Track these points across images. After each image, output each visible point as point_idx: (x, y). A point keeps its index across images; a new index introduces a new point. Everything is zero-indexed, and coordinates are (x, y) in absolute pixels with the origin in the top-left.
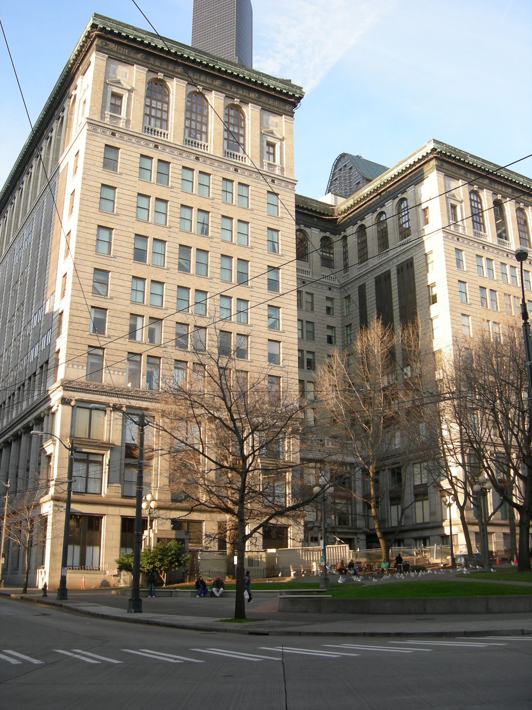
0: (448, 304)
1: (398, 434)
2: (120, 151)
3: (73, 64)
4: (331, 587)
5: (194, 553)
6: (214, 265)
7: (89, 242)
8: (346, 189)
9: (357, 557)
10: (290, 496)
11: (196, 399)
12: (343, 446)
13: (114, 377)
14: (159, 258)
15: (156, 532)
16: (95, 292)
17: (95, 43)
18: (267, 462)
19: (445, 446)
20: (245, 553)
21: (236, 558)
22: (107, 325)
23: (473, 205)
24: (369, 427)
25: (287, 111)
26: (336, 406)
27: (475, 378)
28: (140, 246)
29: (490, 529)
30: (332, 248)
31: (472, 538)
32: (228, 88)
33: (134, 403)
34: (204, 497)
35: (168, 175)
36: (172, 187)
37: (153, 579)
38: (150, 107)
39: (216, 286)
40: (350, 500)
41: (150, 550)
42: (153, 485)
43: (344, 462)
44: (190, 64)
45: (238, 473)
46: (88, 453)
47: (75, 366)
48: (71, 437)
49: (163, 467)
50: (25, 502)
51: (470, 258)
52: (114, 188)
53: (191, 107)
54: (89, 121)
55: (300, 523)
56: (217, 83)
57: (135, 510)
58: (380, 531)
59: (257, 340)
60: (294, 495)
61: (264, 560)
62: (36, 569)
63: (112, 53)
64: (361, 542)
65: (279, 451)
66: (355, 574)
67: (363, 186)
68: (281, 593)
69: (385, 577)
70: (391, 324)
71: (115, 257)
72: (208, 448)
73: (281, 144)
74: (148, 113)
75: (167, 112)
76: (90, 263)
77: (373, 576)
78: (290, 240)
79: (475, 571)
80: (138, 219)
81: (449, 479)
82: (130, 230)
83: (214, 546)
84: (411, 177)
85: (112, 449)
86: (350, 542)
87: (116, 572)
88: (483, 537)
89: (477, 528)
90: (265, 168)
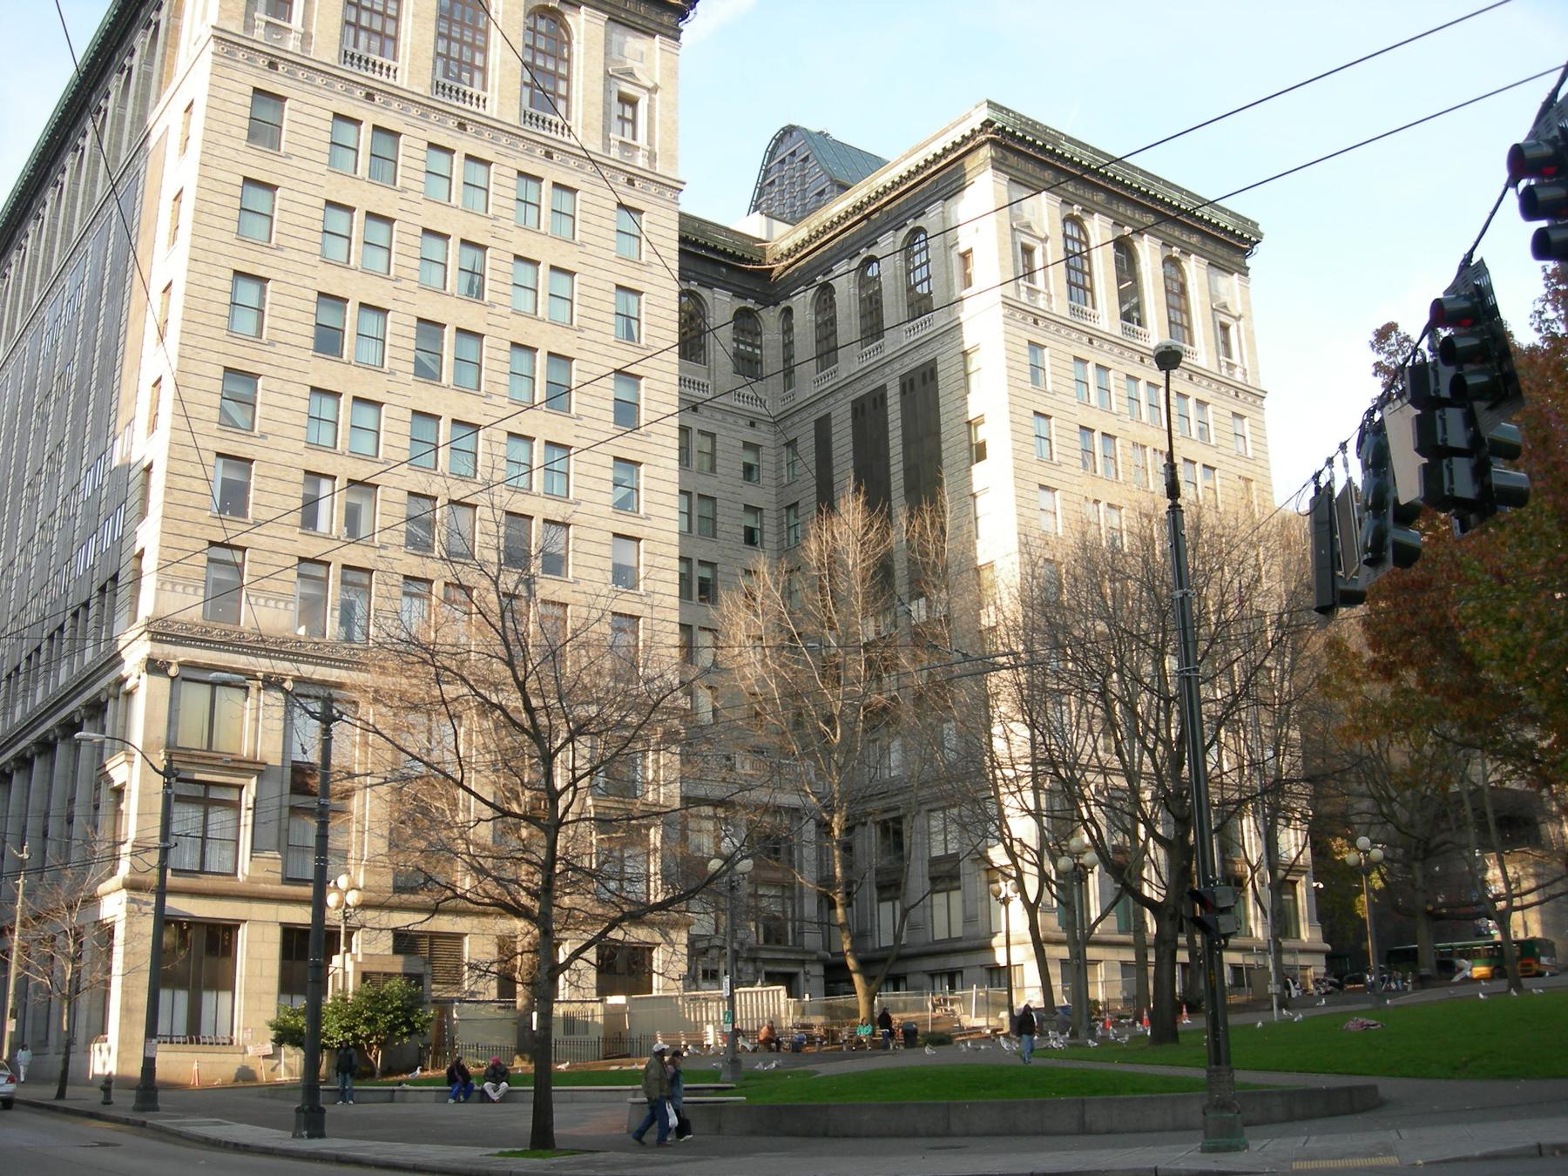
1: (896, 745)
2: (287, 104)
4: (747, 1079)
5: (444, 1005)
7: (213, 307)
8: (792, 206)
9: (803, 1014)
13: (268, 611)
14: (370, 351)
16: (226, 421)
19: (998, 772)
22: (251, 495)
26: (762, 681)
27: (1065, 626)
28: (329, 319)
31: (1055, 971)
33: (307, 670)
40: (789, 890)
42: (352, 854)
45: (542, 827)
46: (207, 784)
47: (179, 588)
48: (168, 746)
51: (1061, 364)
59: (588, 534)
60: (666, 878)
61: (600, 1020)
62: (89, 1042)
65: (634, 781)
71: (271, 343)
75: (396, 19)
78: (665, 313)
82: (308, 282)
83: (491, 990)
84: (937, 181)
85: (261, 775)
86: (791, 983)
88: (1077, 970)
89: (1063, 952)
90: (615, 153)
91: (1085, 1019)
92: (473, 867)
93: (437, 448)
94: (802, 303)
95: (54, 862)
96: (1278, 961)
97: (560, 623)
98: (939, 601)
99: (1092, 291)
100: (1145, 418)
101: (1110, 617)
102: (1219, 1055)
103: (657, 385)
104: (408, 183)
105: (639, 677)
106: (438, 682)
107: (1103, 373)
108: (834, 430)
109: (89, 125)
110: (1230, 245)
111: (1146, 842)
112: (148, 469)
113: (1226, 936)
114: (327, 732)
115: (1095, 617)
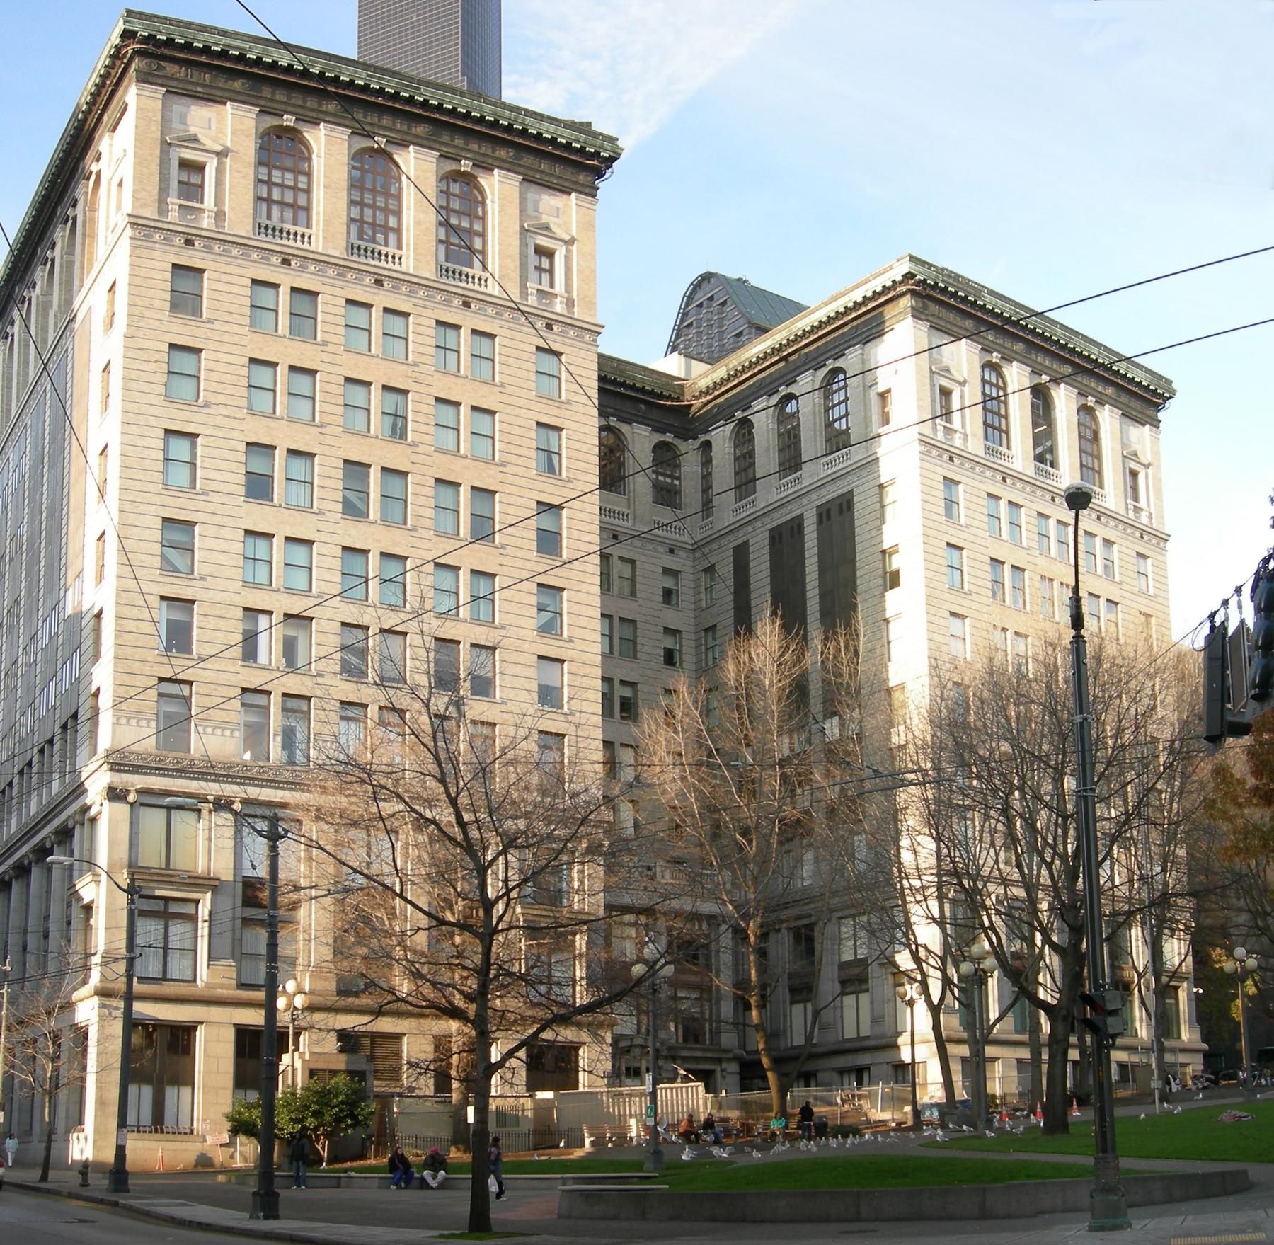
0: (923, 590)
1: (809, 856)
2: (206, 275)
3: (89, 111)
4: (668, 1168)
5: (385, 1100)
6: (421, 501)
7: (148, 464)
8: (710, 346)
9: (720, 1108)
10: (584, 983)
11: (383, 782)
12: (694, 879)
13: (216, 740)
14: (300, 493)
15: (307, 1057)
16: (168, 567)
17: (134, 66)
18: (535, 912)
19: (905, 882)
20: (491, 1100)
21: (471, 1111)
22: (195, 634)
23: (987, 391)
24: (750, 842)
25: (583, 185)
26: (681, 795)
27: (971, 746)
28: (258, 466)
29: (990, 1051)
30: (678, 466)
31: (956, 1068)
32: (446, 139)
33: (254, 792)
34: (405, 985)
35: (315, 319)
36: (324, 343)
37: (301, 1151)
38: (269, 183)
39: (426, 544)
40: (706, 991)
41: (294, 1094)
42: (300, 961)
43: (695, 914)
44: (356, 95)
45: (476, 934)
46: (167, 900)
47: (134, 722)
48: (130, 866)
49: (320, 925)
50: (42, 999)
51: (975, 499)
52: (198, 351)
53: (362, 179)
54: (134, 220)
55: (603, 1038)
56: (421, 129)
57: (263, 1012)
58: (768, 1056)
59: (514, 657)
60: (591, 981)
61: (529, 1114)
62: (68, 1132)
63: (174, 84)
64: (729, 1078)
65: (560, 891)
66: (717, 1142)
67: (750, 340)
68: (564, 1181)
69: (778, 1148)
70: (799, 628)
71: (205, 493)
72: (413, 883)
73: (567, 251)
74: (265, 195)
75: (308, 191)
76: (153, 508)
77: (753, 1147)
78: (585, 448)
79: (960, 1135)
80: (252, 412)
81: (911, 950)
82: (236, 435)
83: (427, 1085)
84: (856, 327)
85: (214, 889)
86: (706, 1077)
87: (225, 1138)
88: (977, 1067)
89: (964, 1050)
90: (532, 300)
91: (983, 1111)
92: (411, 972)
93: (367, 581)
94: (721, 436)
95: (33, 973)
96: (1160, 1060)
97: (489, 742)
98: (851, 720)
99: (1007, 432)
100: (1053, 554)
101: (1014, 738)
102: (1105, 1144)
103: (580, 515)
104: (329, 338)
105: (565, 792)
106: (375, 800)
107: (1015, 509)
108: (752, 557)
109: (16, 314)
110: (1144, 398)
111: (1042, 949)
112: (98, 616)
113: (1114, 1037)
114: (274, 848)
115: (999, 738)
